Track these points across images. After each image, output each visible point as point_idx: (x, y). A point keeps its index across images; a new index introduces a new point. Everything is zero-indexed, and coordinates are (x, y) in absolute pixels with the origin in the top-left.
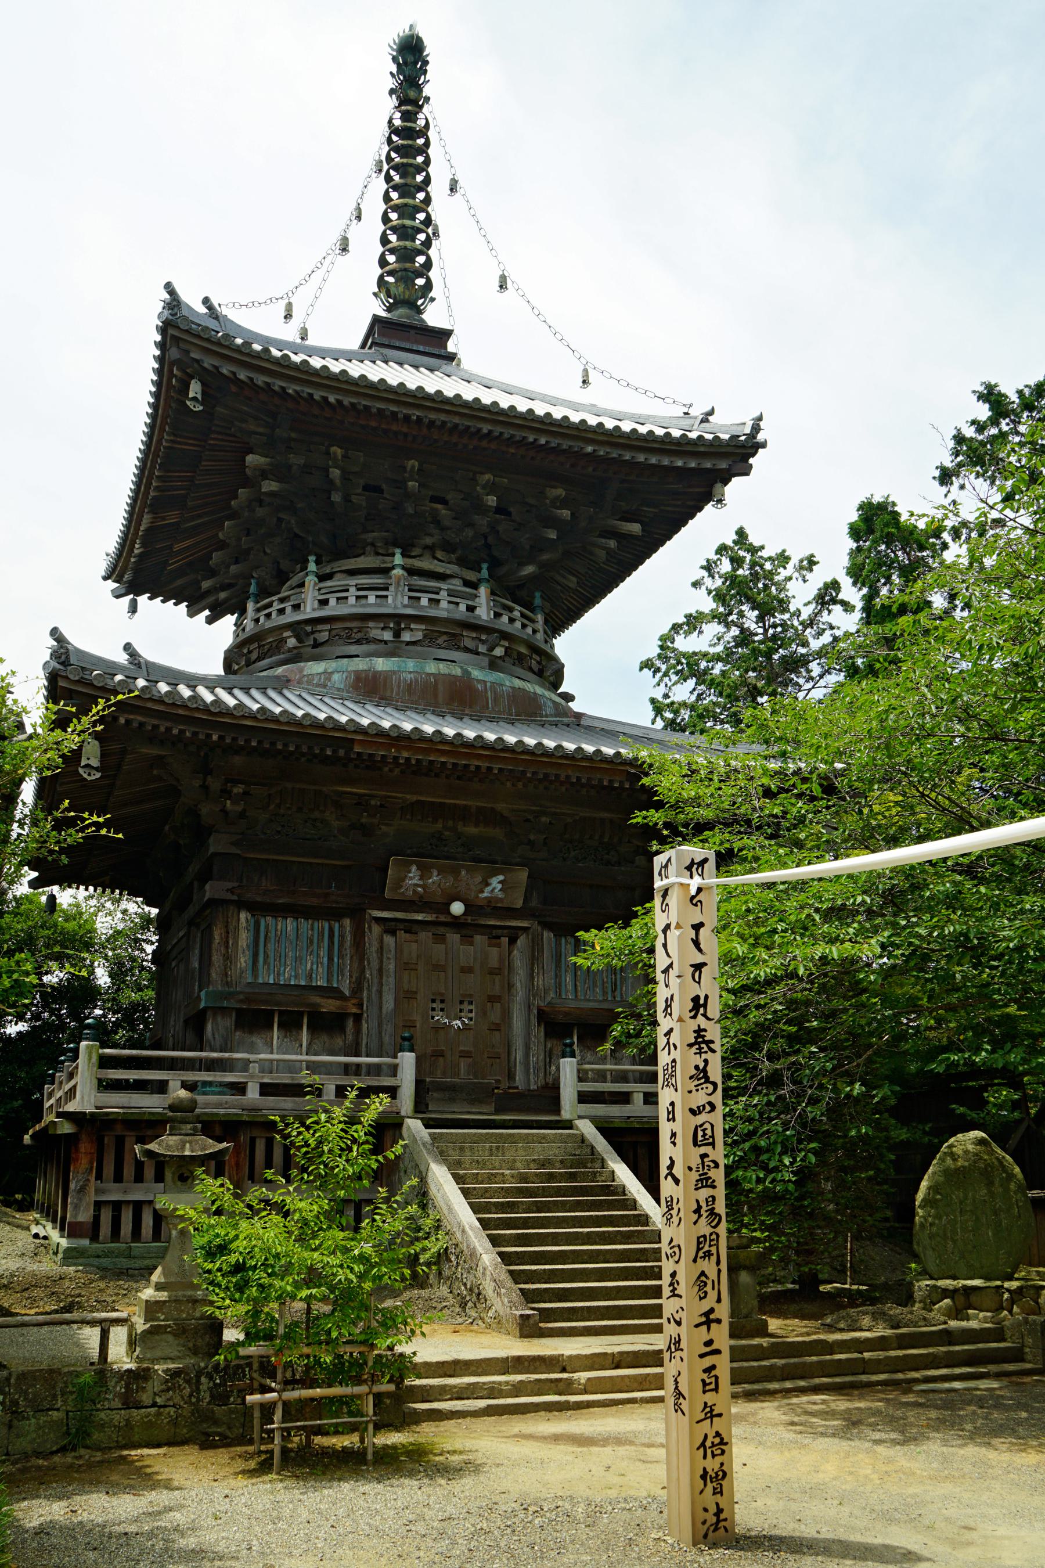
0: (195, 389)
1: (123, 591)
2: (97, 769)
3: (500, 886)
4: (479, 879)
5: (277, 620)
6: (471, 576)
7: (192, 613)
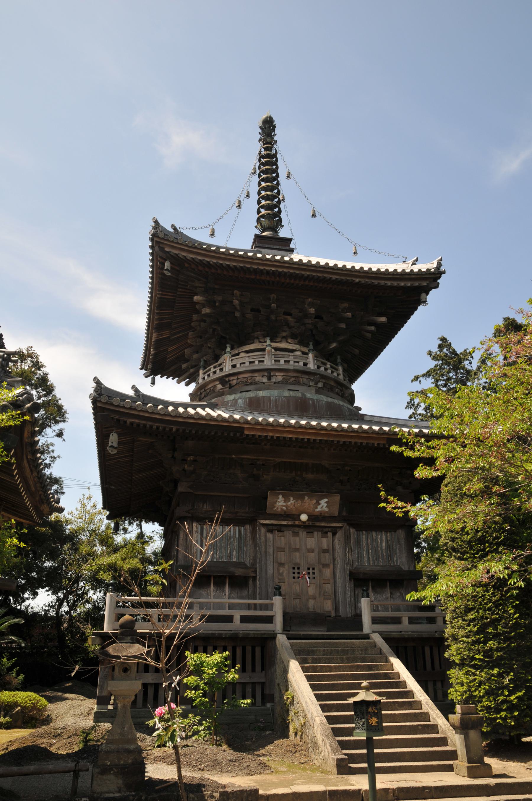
0: (167, 265)
1: (149, 374)
2: (116, 448)
3: (326, 505)
4: (314, 501)
5: (213, 377)
6: (305, 350)
7: (179, 382)
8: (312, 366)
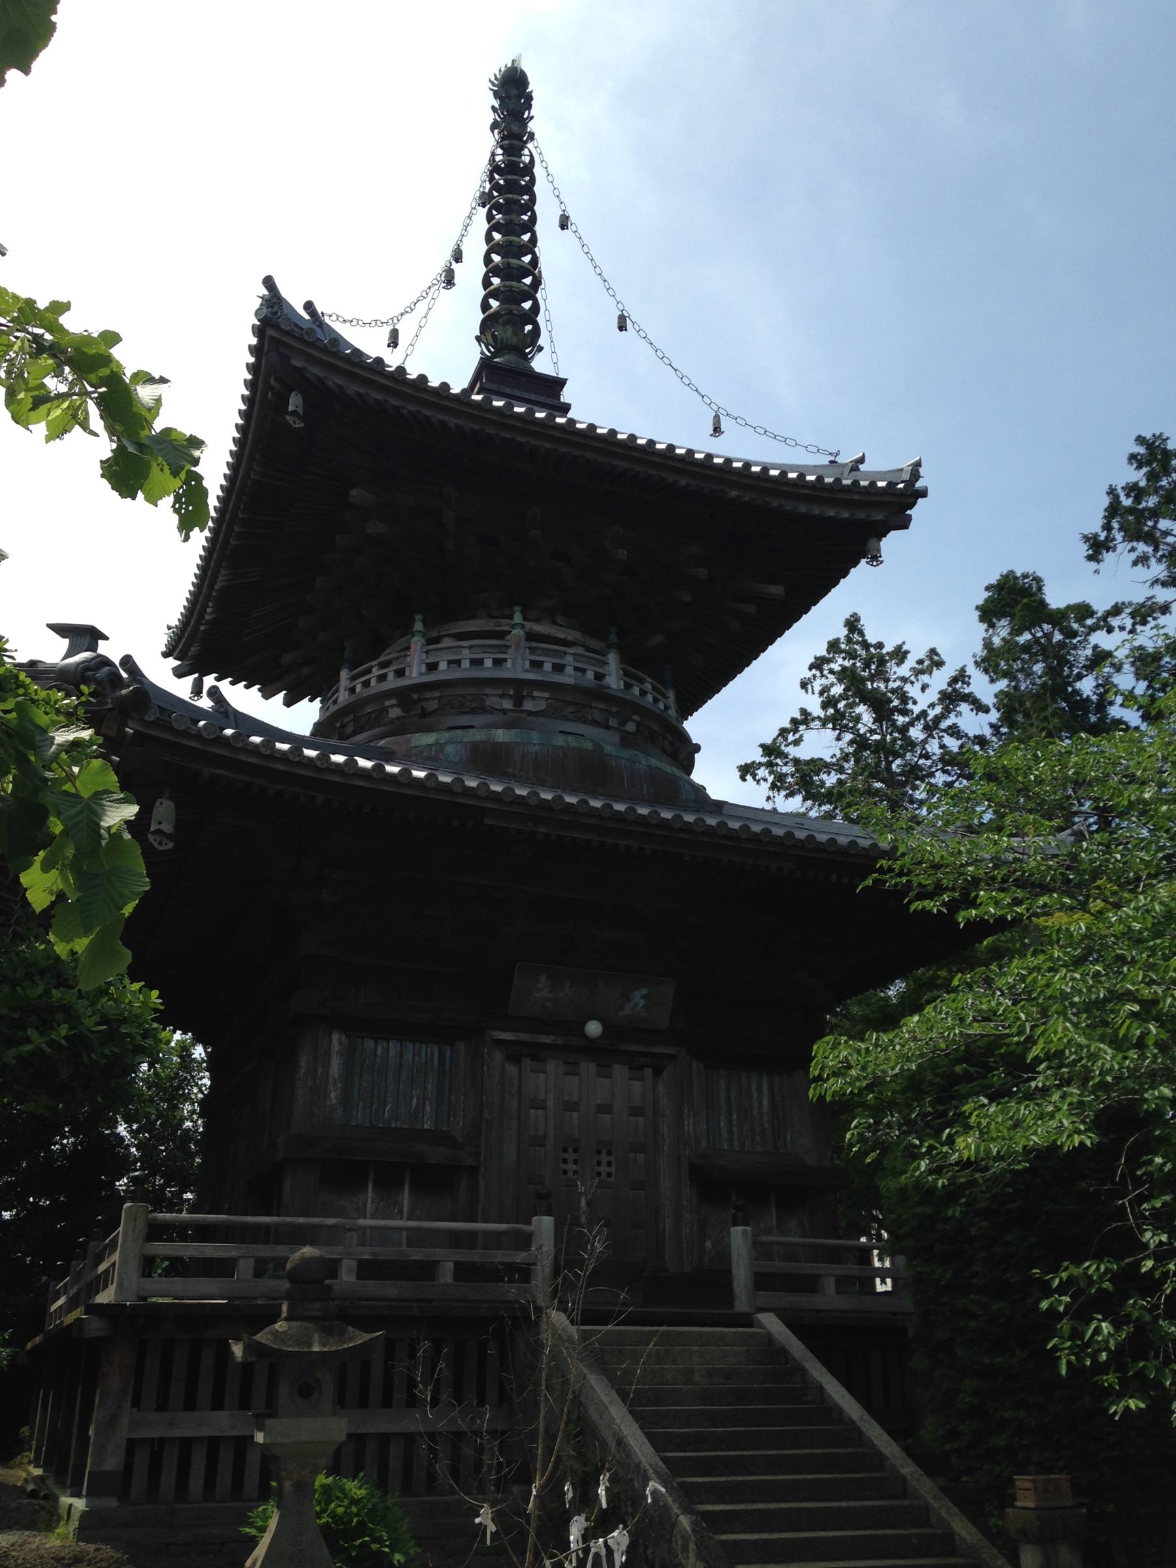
0: (295, 402)
1: (186, 669)
2: (169, 837)
3: (642, 1002)
5: (376, 687)
6: (595, 644)
8: (614, 681)
